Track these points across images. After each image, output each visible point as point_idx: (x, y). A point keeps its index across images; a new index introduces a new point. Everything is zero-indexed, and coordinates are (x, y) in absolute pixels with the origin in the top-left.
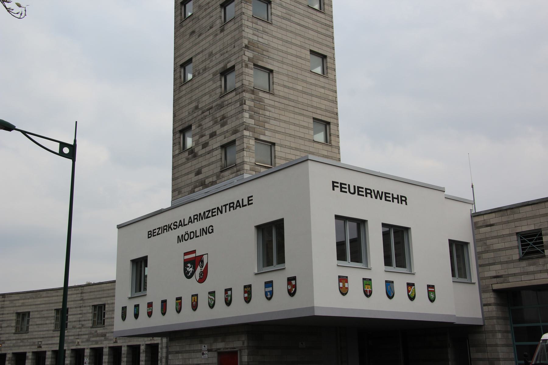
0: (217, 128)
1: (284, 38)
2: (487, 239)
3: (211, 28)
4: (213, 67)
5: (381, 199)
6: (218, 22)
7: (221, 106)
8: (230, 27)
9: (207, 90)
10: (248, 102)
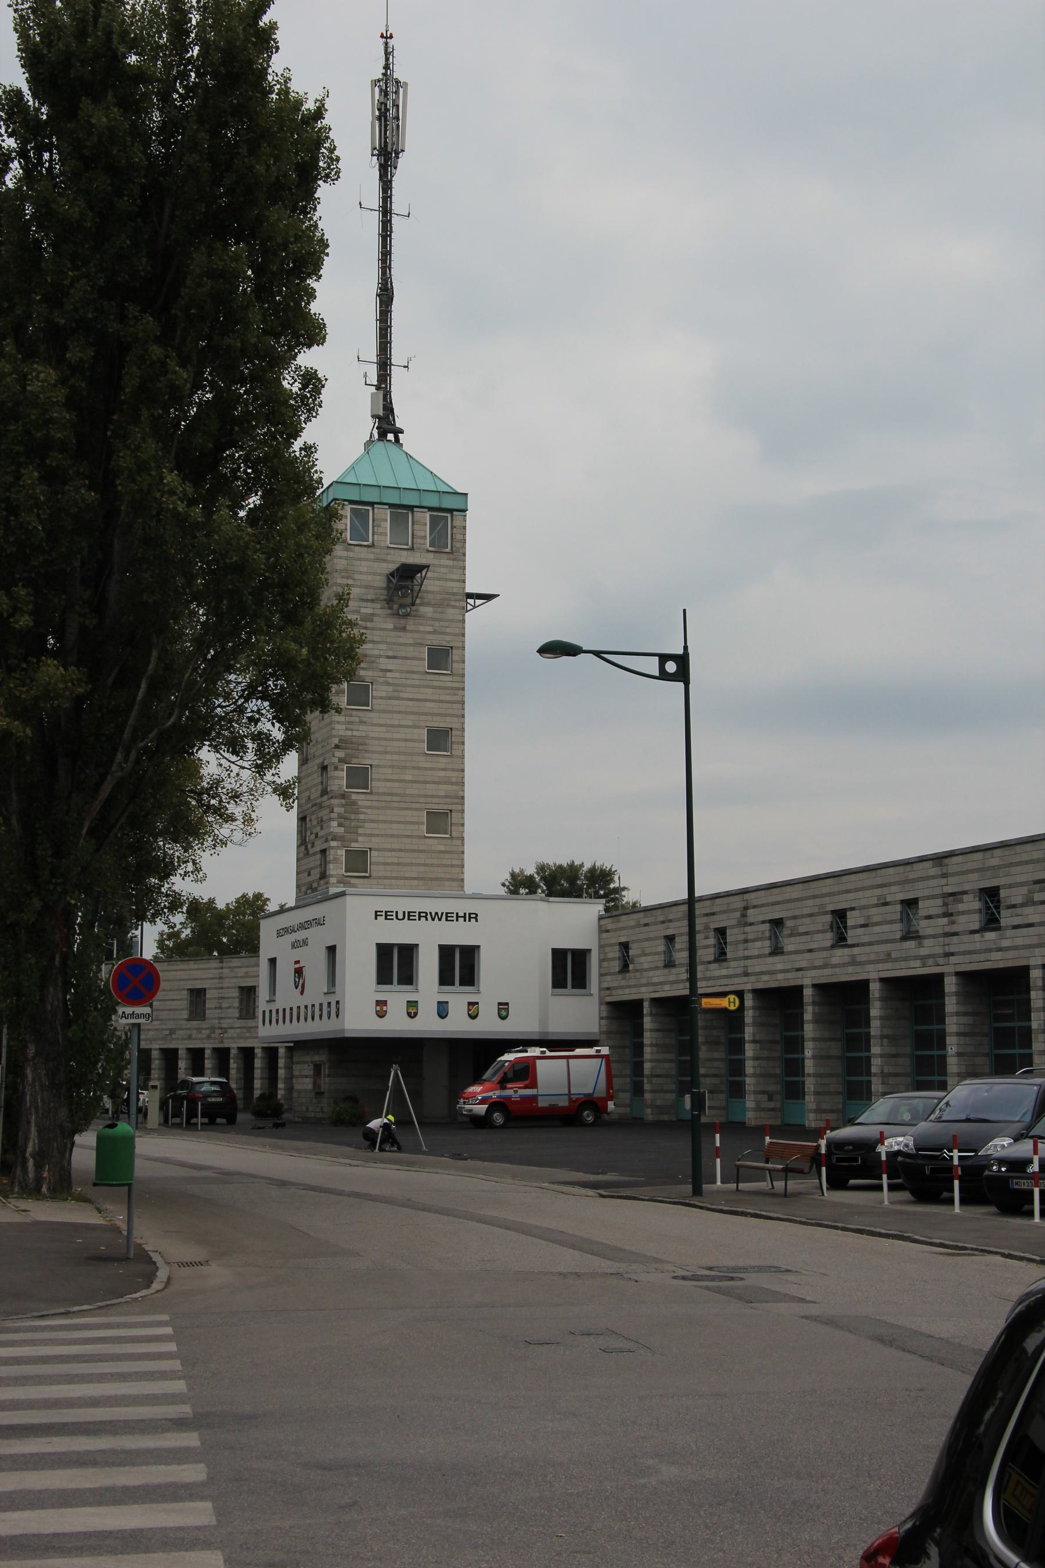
5: (440, 920)
10: (336, 810)
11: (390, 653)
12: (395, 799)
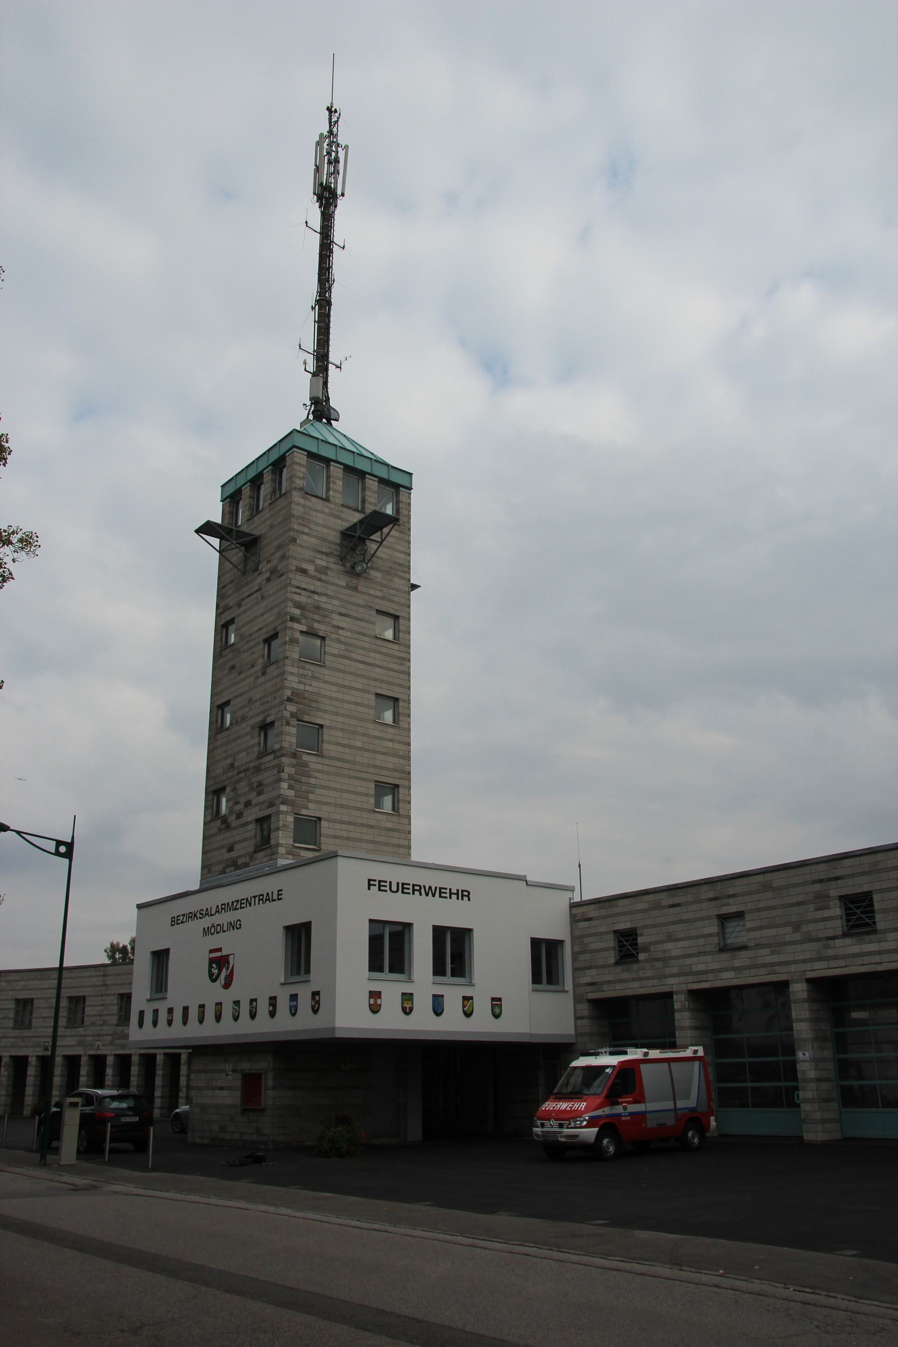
0: (252, 796)
1: (341, 682)
2: (585, 936)
3: (253, 666)
4: (252, 718)
5: (434, 895)
6: (260, 661)
7: (258, 769)
8: (273, 670)
9: (244, 746)
10: (287, 769)
11: (343, 611)
12: (345, 765)
